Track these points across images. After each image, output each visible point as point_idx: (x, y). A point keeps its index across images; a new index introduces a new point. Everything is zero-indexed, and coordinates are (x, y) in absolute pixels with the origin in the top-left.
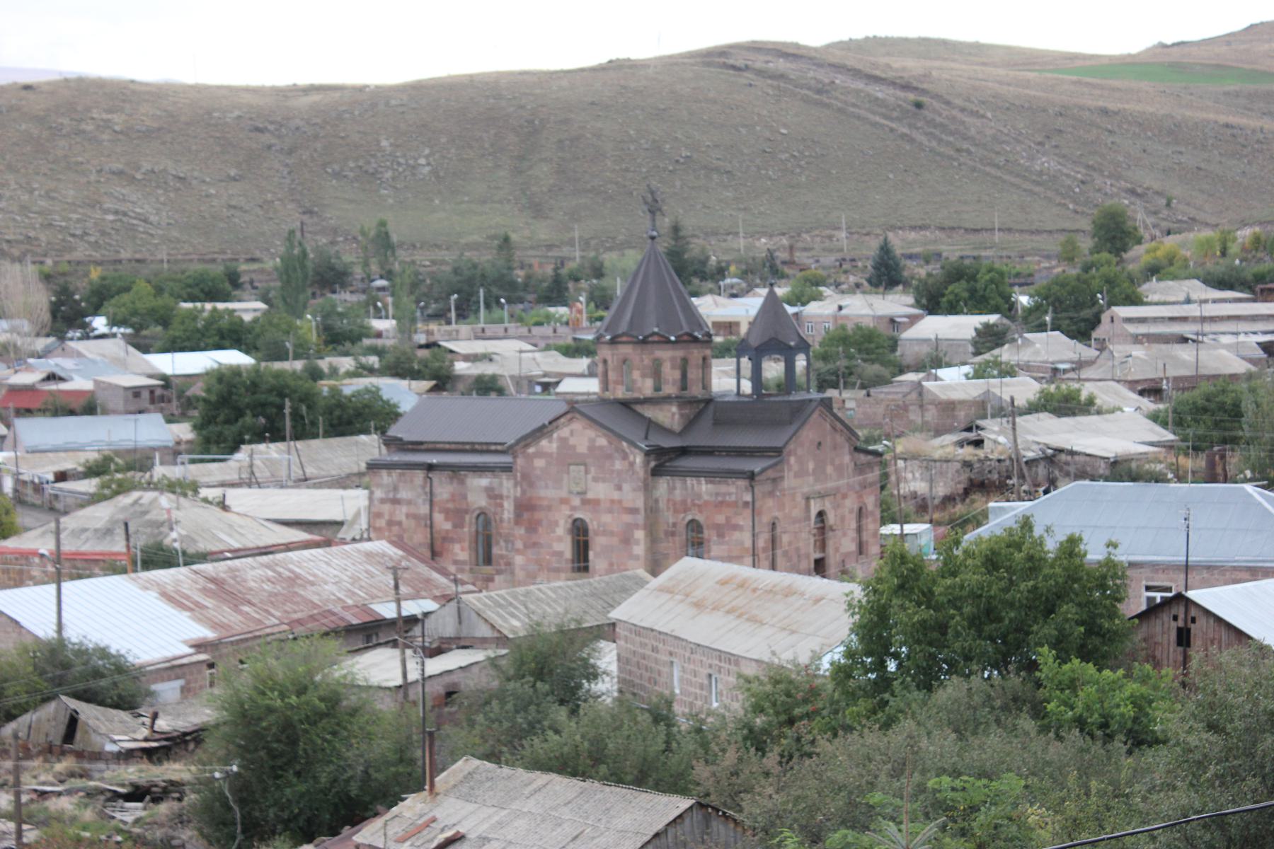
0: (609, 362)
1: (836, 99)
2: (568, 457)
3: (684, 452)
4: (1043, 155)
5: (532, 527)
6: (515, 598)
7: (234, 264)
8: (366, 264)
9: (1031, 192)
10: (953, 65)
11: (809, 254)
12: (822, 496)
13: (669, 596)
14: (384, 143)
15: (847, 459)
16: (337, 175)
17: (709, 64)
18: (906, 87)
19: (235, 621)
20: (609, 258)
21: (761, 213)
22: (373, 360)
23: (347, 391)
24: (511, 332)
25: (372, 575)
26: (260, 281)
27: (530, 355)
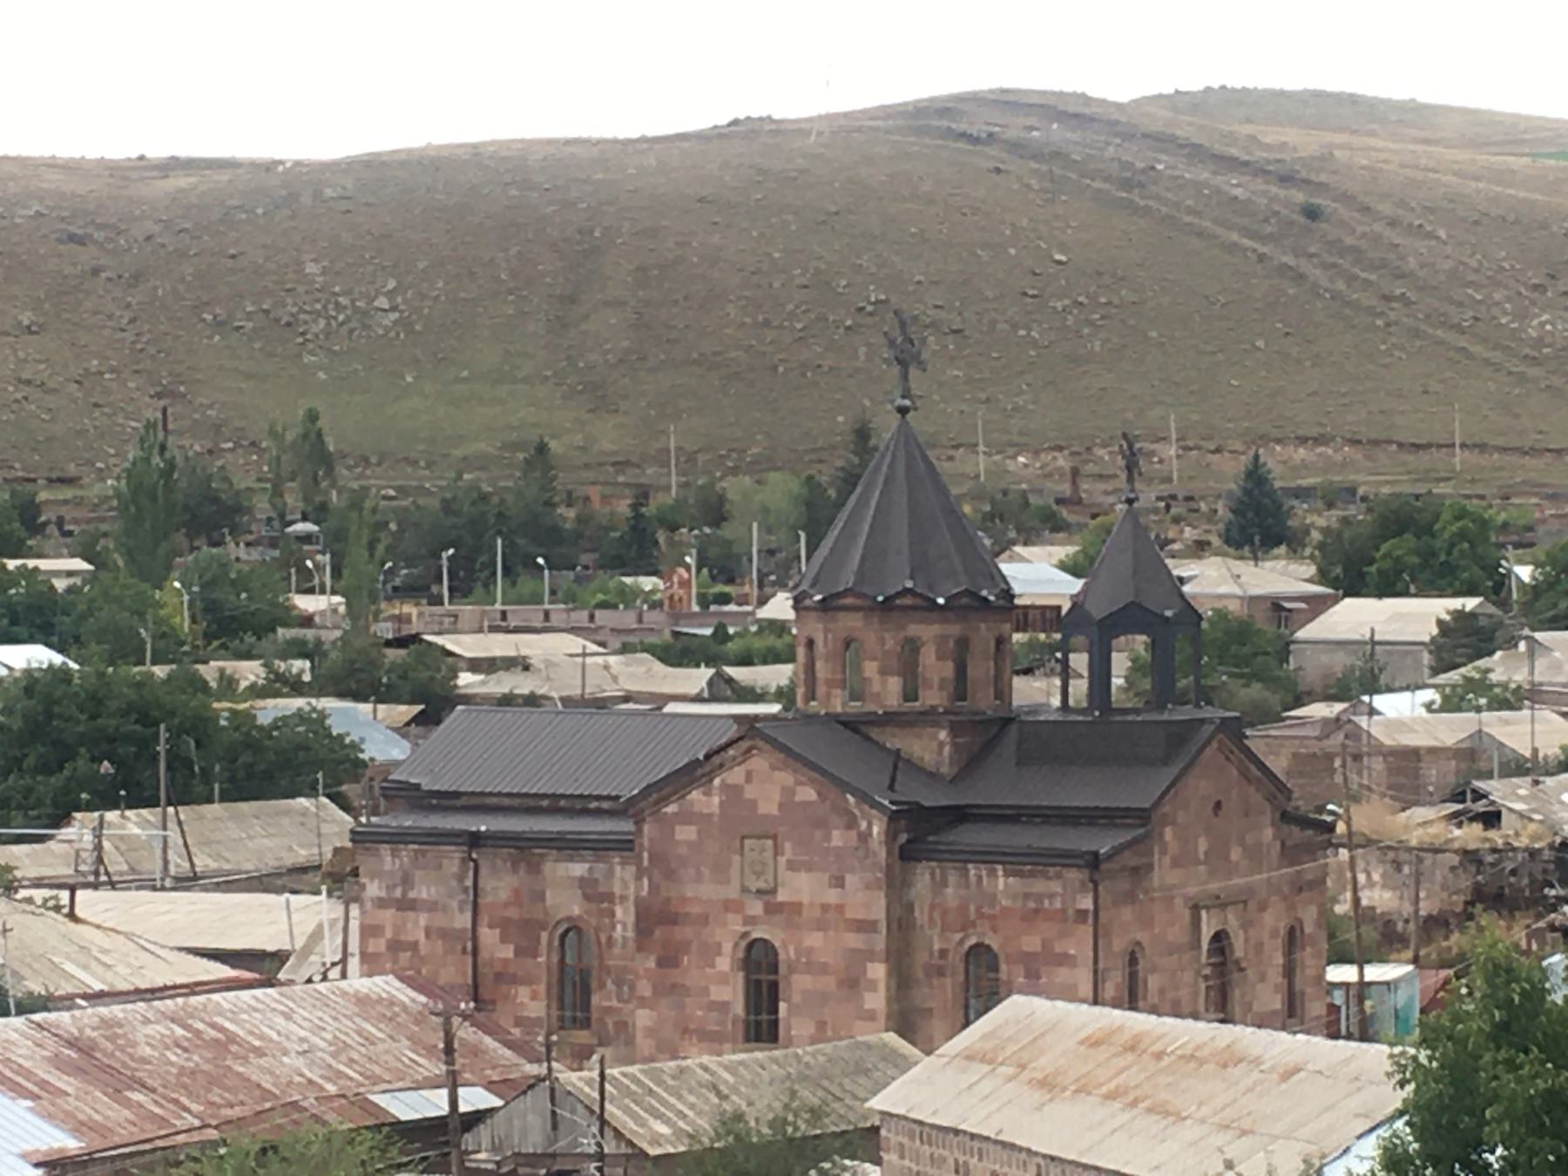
0: (820, 643)
1: (1158, 198)
2: (742, 827)
3: (960, 815)
4: (1543, 310)
5: (668, 961)
6: (660, 1083)
7: (29, 487)
8: (277, 492)
9: (1521, 378)
10: (1372, 141)
11: (1109, 487)
12: (1220, 903)
13: (986, 1068)
14: (311, 268)
15: (1268, 833)
16: (219, 325)
17: (920, 131)
18: (1286, 179)
19: (119, 1120)
20: (734, 488)
21: (1016, 409)
22: (301, 666)
23: (264, 719)
24: (555, 620)
25: (370, 1040)
26: (75, 521)
27: (600, 660)
